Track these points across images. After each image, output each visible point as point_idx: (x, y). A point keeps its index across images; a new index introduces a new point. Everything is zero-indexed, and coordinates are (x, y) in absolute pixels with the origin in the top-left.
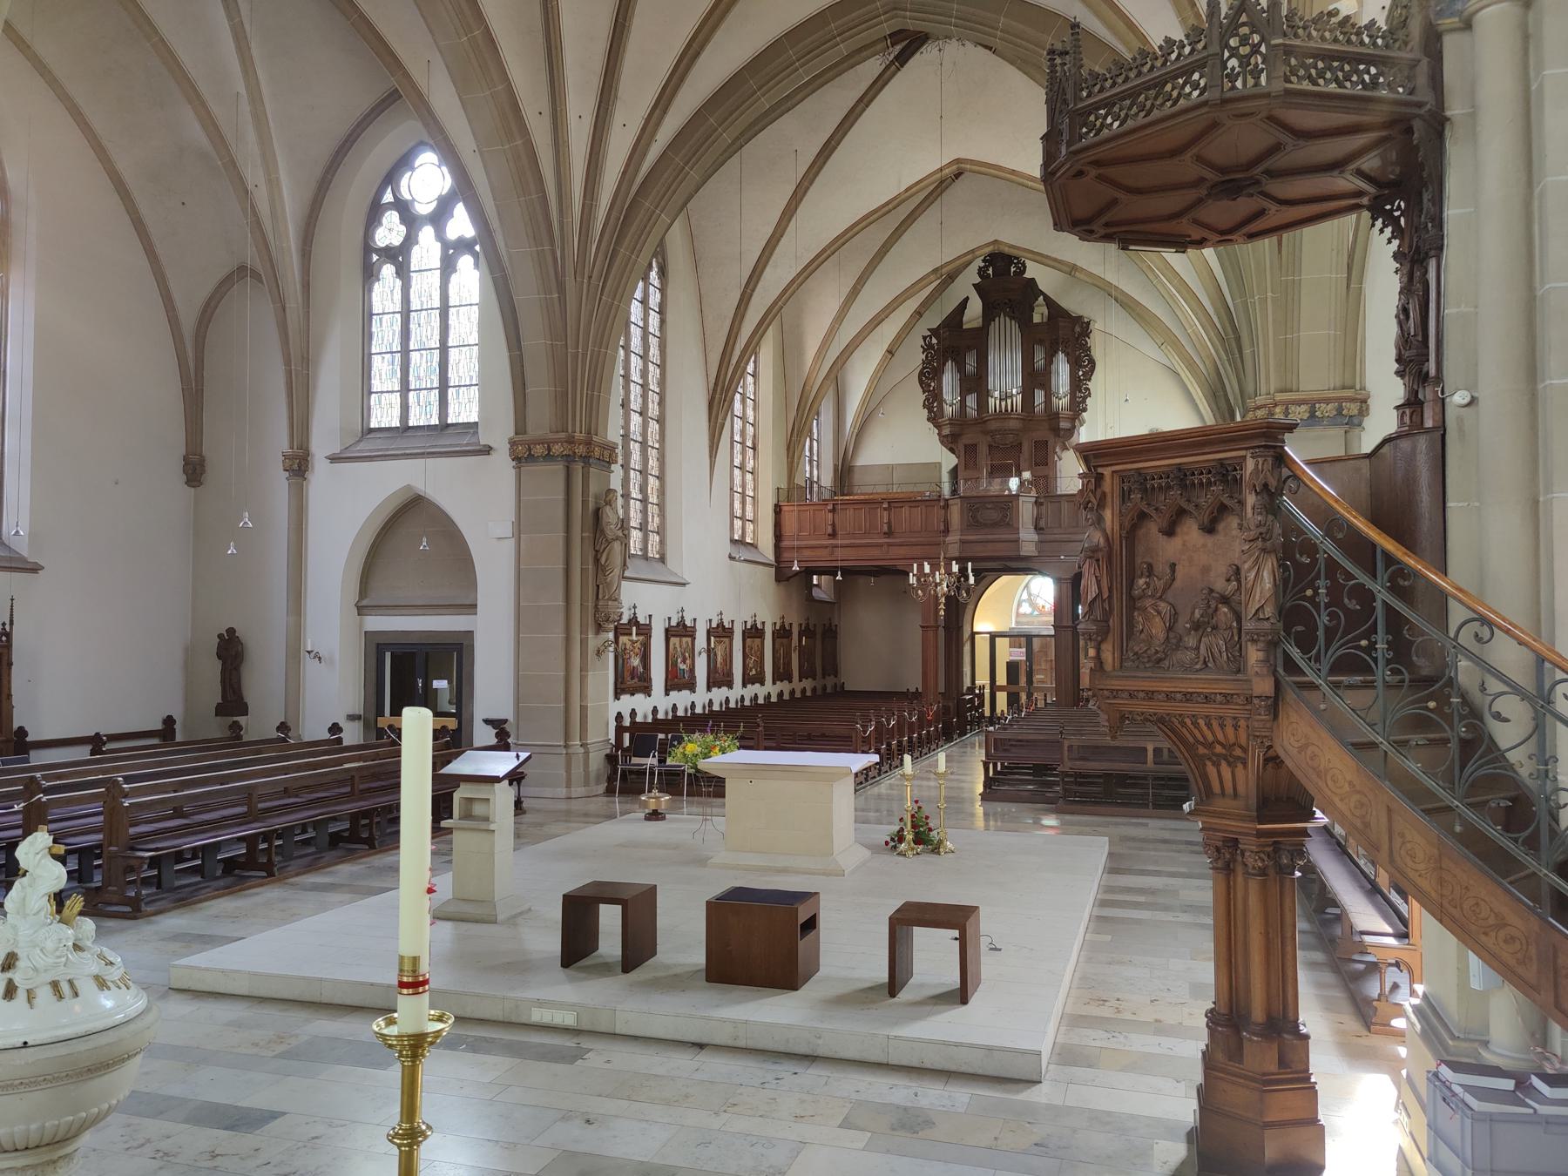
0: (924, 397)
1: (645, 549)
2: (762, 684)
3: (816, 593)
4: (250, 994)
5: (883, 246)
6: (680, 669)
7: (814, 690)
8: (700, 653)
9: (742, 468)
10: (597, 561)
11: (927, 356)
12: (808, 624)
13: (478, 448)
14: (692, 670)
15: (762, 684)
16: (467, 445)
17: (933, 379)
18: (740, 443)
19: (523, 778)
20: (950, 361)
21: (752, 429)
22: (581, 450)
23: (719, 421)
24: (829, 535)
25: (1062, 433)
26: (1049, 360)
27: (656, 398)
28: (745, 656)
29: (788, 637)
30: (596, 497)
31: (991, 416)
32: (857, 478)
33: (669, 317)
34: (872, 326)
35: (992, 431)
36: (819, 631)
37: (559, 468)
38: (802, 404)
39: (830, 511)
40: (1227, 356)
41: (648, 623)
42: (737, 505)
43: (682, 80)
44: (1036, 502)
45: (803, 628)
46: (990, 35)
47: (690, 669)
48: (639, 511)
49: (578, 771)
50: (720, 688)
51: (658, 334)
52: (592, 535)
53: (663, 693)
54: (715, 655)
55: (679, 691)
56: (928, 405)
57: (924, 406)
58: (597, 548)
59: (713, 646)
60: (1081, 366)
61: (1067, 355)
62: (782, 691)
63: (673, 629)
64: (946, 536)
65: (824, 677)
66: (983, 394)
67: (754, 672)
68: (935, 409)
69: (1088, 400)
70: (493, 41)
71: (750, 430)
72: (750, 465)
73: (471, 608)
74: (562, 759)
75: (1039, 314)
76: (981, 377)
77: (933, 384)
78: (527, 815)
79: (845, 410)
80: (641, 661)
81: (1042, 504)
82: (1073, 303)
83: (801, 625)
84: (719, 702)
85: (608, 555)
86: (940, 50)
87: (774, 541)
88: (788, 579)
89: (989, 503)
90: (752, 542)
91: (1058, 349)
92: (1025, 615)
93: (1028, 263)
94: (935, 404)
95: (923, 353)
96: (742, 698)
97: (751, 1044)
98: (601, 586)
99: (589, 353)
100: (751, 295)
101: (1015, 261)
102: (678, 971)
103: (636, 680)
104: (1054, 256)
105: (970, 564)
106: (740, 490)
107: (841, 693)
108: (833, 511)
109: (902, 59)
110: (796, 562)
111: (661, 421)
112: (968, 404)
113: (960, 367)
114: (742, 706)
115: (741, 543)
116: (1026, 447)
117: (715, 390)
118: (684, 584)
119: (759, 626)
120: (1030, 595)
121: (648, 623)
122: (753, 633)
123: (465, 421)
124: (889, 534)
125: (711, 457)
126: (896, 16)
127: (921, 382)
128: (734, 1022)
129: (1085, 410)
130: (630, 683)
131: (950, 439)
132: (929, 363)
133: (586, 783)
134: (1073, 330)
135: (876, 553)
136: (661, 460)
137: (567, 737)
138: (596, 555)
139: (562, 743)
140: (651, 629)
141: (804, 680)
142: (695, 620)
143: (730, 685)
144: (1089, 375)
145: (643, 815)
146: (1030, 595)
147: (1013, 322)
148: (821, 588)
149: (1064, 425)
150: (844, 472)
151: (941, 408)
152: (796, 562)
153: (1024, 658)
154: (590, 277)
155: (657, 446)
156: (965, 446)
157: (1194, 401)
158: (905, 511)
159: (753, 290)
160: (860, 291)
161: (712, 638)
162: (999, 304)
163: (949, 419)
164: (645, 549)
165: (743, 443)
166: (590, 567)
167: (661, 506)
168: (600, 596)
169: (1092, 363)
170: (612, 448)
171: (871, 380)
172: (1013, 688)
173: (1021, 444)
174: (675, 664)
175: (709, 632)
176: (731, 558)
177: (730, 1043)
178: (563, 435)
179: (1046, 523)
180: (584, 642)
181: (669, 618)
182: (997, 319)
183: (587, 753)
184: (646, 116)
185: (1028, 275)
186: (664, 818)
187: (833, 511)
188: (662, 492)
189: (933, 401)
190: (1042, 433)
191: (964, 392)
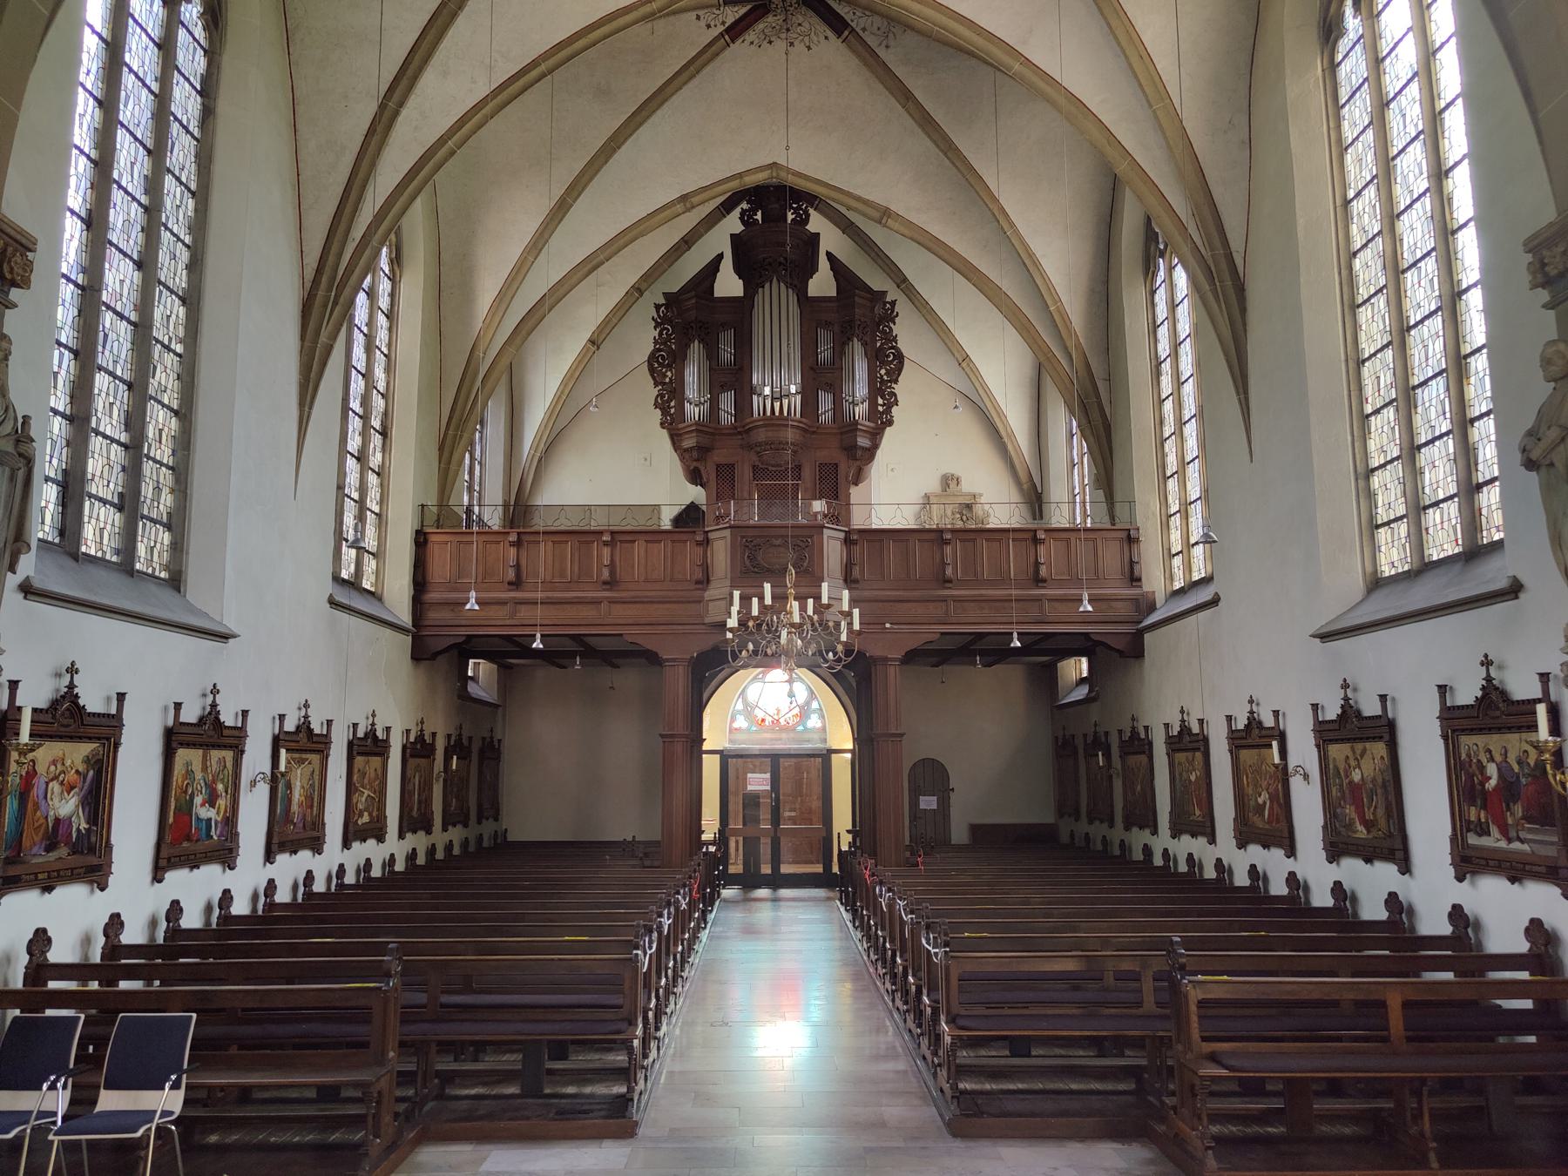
0: (655, 392)
1: (127, 549)
2: (380, 838)
3: (472, 688)
5: (611, 139)
6: (198, 819)
7: (465, 844)
8: (253, 783)
9: (361, 458)
11: (661, 334)
12: (460, 735)
14: (230, 821)
15: (380, 838)
17: (669, 366)
18: (360, 417)
20: (696, 342)
21: (373, 563)
23: (323, 338)
24: (509, 583)
25: (859, 453)
27: (184, 256)
28: (350, 789)
29: (429, 757)
33: (223, 106)
34: (579, 275)
36: (475, 748)
39: (512, 544)
41: (113, 711)
42: (349, 520)
45: (452, 743)
48: (117, 468)
50: (295, 852)
51: (194, 127)
53: (148, 877)
54: (289, 786)
55: (192, 868)
56: (662, 405)
57: (656, 405)
59: (282, 768)
60: (884, 363)
61: (865, 344)
62: (414, 850)
63: (184, 730)
65: (479, 822)
66: (746, 395)
67: (366, 818)
68: (673, 411)
69: (894, 409)
71: (378, 403)
72: (376, 460)
75: (822, 284)
76: (741, 369)
77: (669, 374)
79: (522, 424)
80: (84, 802)
81: (854, 543)
83: (449, 736)
84: (290, 883)
87: (412, 592)
88: (434, 656)
89: (777, 537)
90: (373, 589)
94: (672, 404)
95: (655, 329)
96: (341, 870)
101: (795, 206)
103: (63, 851)
104: (858, 192)
106: (355, 495)
107: (503, 848)
108: (518, 544)
112: (722, 406)
113: (712, 353)
114: (341, 886)
115: (353, 585)
116: (807, 473)
118: (224, 637)
119: (380, 734)
120: (746, 703)
121: (113, 711)
122: (368, 746)
124: (611, 584)
125: (301, 404)
127: (652, 370)
129: (890, 423)
131: (695, 454)
132: (665, 344)
135: (587, 613)
141: (450, 828)
142: (245, 713)
143: (316, 845)
146: (746, 703)
148: (477, 682)
150: (518, 510)
151: (681, 407)
153: (769, 788)
155: (179, 348)
156: (718, 466)
157: (1001, 438)
158: (639, 548)
159: (401, 104)
160: (571, 206)
161: (283, 752)
162: (770, 264)
163: (697, 424)
164: (127, 549)
165: (365, 418)
167: (181, 472)
171: (564, 383)
174: (186, 809)
175: (276, 742)
176: (333, 603)
181: (178, 706)
182: (767, 286)
187: (518, 544)
188: (184, 443)
189: (669, 399)
190: (830, 453)
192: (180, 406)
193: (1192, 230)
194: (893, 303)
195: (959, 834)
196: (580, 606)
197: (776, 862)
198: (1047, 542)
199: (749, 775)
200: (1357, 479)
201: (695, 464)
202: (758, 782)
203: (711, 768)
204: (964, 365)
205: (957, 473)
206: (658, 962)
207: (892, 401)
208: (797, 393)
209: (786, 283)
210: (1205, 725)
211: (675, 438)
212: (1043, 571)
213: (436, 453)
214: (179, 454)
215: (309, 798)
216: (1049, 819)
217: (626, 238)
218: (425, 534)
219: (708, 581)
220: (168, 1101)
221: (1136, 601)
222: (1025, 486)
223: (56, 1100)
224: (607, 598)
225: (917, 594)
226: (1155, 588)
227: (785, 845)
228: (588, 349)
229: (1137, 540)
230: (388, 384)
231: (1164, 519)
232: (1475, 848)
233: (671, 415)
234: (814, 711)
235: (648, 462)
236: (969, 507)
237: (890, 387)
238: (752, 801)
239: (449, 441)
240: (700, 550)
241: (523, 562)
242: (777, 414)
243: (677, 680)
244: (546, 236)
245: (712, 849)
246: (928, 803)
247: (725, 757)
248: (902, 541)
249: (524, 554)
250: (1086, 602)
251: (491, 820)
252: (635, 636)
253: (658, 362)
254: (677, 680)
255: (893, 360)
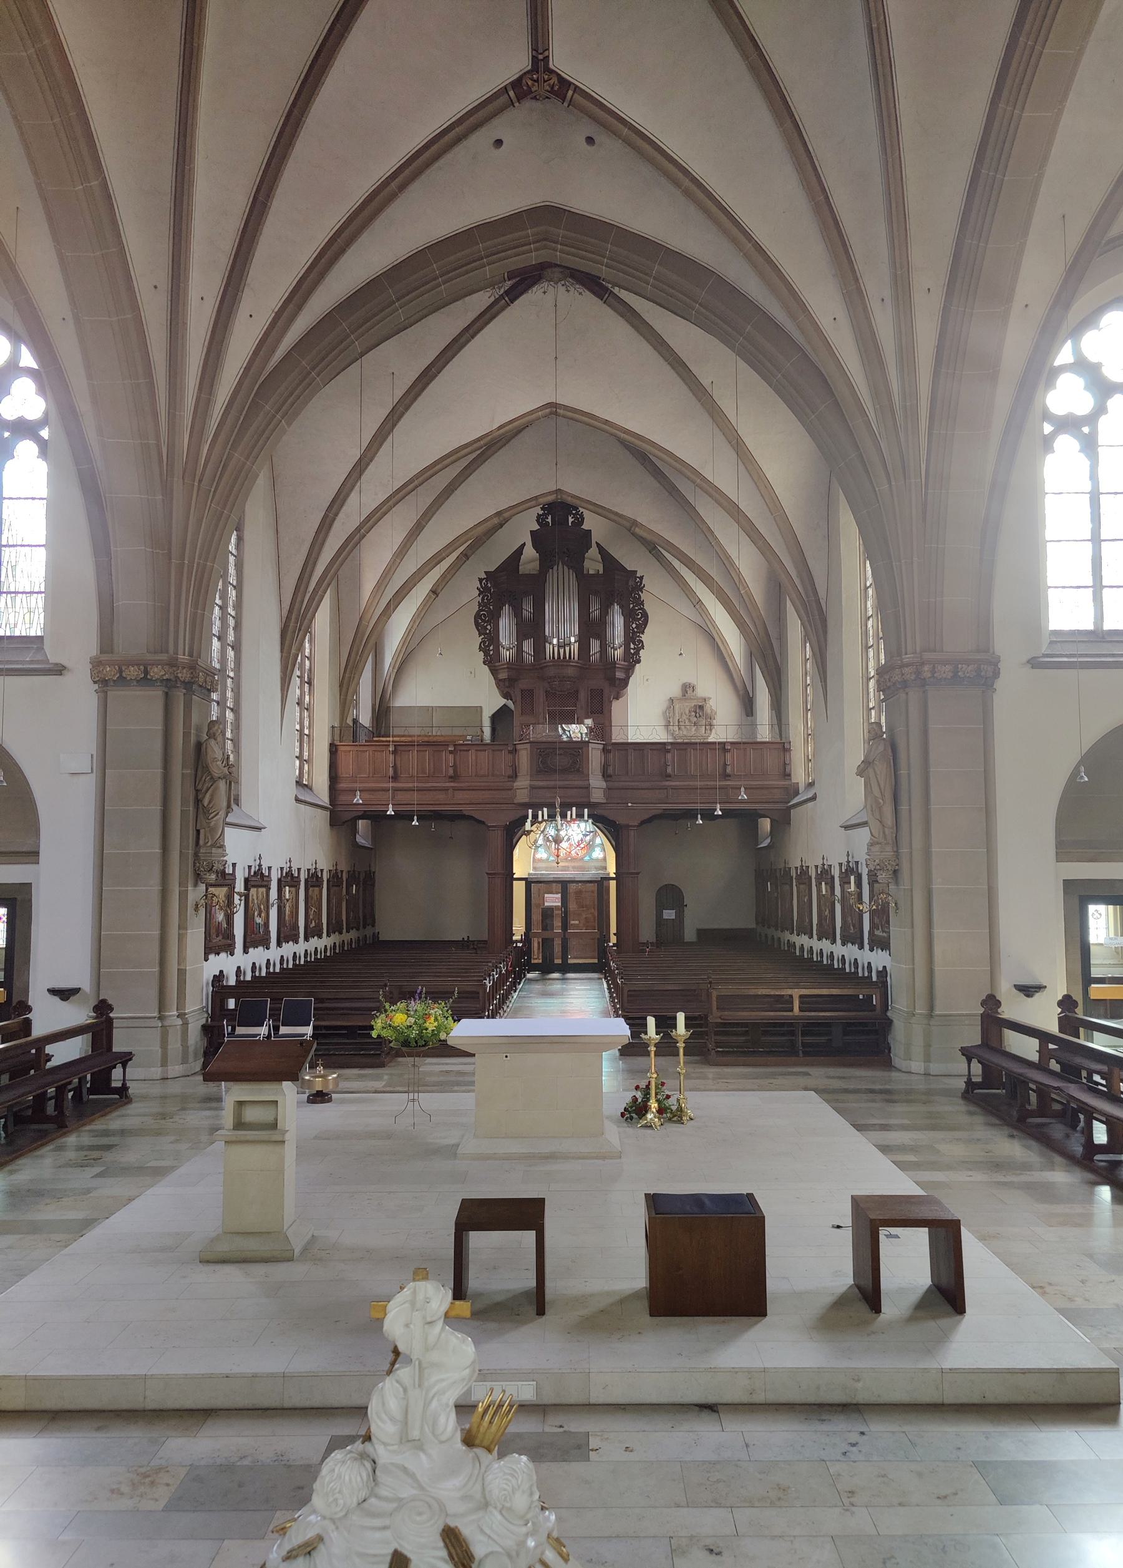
0: (480, 639)
2: (320, 937)
4: (28, 1408)
5: (450, 484)
10: (198, 801)
11: (483, 599)
13: (47, 666)
14: (267, 924)
15: (320, 937)
16: (31, 662)
17: (489, 622)
19: (130, 1059)
22: (184, 675)
23: (293, 651)
25: (617, 682)
26: (605, 610)
30: (199, 729)
31: (549, 662)
32: (394, 719)
35: (551, 678)
37: (158, 693)
38: (357, 641)
40: (808, 617)
41: (231, 872)
43: (322, 275)
44: (603, 749)
46: (640, 279)
47: (265, 923)
49: (174, 1044)
50: (219, 954)
52: (193, 772)
56: (483, 648)
58: (199, 787)
60: (635, 619)
64: (514, 782)
68: (491, 653)
69: (642, 652)
70: (109, 197)
73: (32, 856)
74: (156, 1035)
75: (593, 564)
77: (489, 627)
78: (133, 1105)
81: (609, 751)
82: (631, 559)
85: (212, 795)
86: (545, 292)
91: (614, 601)
92: (541, 860)
93: (586, 514)
94: (491, 648)
97: (772, 1398)
98: (202, 832)
99: (195, 565)
100: (334, 519)
101: (574, 512)
102: (500, 1298)
103: (220, 938)
104: (615, 509)
105: (586, 810)
107: (377, 945)
108: (395, 752)
109: (513, 295)
110: (391, 806)
111: (237, 647)
112: (524, 607)
113: (517, 612)
116: (583, 695)
117: (288, 618)
118: (259, 829)
123: (24, 634)
124: (454, 778)
125: (282, 690)
126: (545, 247)
127: (477, 625)
128: (749, 1372)
129: (639, 661)
130: (217, 940)
131: (507, 684)
133: (184, 1060)
134: (627, 583)
135: (441, 797)
136: (235, 690)
137: (162, 1007)
138: (197, 796)
139: (156, 1014)
140: (235, 879)
144: (642, 628)
145: (306, 1096)
147: (571, 571)
149: (620, 675)
150: (382, 711)
152: (391, 806)
153: (560, 904)
154: (200, 481)
158: (471, 755)
159: (336, 515)
163: (508, 663)
166: (191, 809)
168: (201, 842)
169: (645, 616)
170: (210, 672)
171: (413, 620)
172: (547, 935)
173: (577, 692)
177: (745, 1399)
178: (164, 657)
179: (614, 769)
180: (183, 896)
182: (555, 567)
183: (185, 1024)
184: (276, 310)
185: (585, 527)
186: (330, 1100)
191: (521, 636)
192: (234, 706)
193: (797, 581)
194: (641, 578)
195: (690, 935)
196: (434, 793)
197: (564, 957)
198: (732, 750)
199: (546, 895)
200: (864, 743)
201: (507, 690)
202: (553, 900)
203: (519, 889)
204: (697, 606)
205: (693, 681)
206: (496, 987)
207: (640, 646)
208: (575, 642)
209: (567, 566)
210: (859, 865)
211: (494, 672)
212: (729, 770)
213: (338, 689)
214: (234, 731)
215: (292, 912)
216: (754, 926)
217: (459, 542)
218: (336, 746)
219: (516, 776)
220: (308, 1030)
221: (786, 789)
222: (741, 693)
223: (263, 1031)
224: (452, 787)
225: (647, 785)
226: (799, 781)
227: (573, 943)
228: (430, 597)
229: (789, 750)
230: (311, 650)
231: (806, 736)
232: (877, 936)
233: (490, 656)
234: (598, 846)
235: (473, 675)
236: (701, 707)
237: (639, 636)
238: (547, 913)
239: (345, 682)
240: (511, 756)
241: (398, 763)
242: (562, 658)
243: (497, 839)
244: (408, 547)
245: (520, 945)
246: (669, 914)
247: (529, 882)
248: (640, 750)
249: (398, 758)
250: (718, 810)
251: (370, 926)
252: (467, 810)
253: (481, 619)
254: (497, 839)
255: (641, 618)
